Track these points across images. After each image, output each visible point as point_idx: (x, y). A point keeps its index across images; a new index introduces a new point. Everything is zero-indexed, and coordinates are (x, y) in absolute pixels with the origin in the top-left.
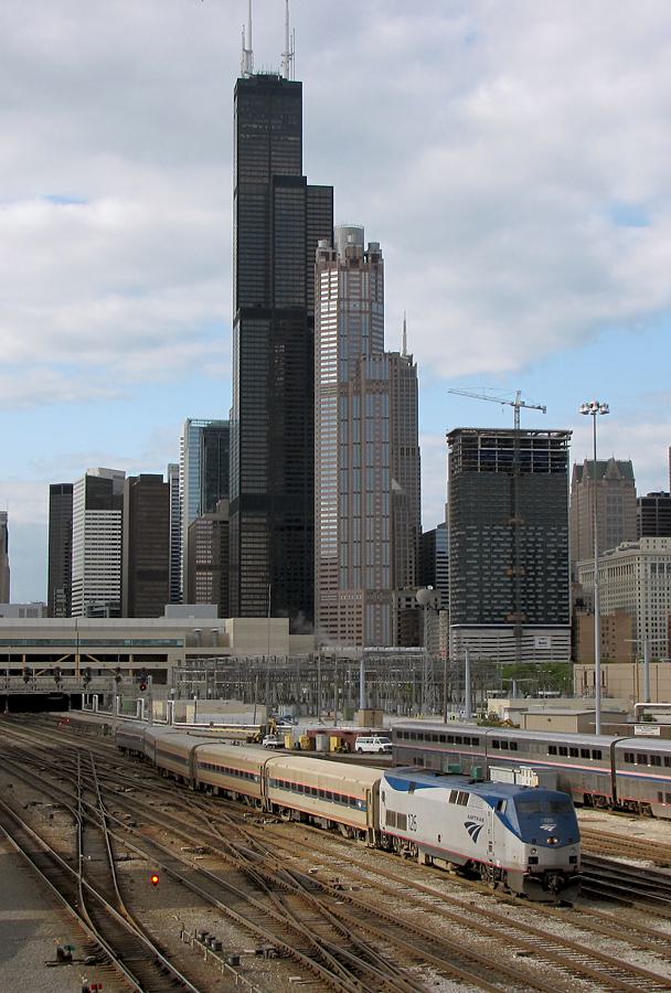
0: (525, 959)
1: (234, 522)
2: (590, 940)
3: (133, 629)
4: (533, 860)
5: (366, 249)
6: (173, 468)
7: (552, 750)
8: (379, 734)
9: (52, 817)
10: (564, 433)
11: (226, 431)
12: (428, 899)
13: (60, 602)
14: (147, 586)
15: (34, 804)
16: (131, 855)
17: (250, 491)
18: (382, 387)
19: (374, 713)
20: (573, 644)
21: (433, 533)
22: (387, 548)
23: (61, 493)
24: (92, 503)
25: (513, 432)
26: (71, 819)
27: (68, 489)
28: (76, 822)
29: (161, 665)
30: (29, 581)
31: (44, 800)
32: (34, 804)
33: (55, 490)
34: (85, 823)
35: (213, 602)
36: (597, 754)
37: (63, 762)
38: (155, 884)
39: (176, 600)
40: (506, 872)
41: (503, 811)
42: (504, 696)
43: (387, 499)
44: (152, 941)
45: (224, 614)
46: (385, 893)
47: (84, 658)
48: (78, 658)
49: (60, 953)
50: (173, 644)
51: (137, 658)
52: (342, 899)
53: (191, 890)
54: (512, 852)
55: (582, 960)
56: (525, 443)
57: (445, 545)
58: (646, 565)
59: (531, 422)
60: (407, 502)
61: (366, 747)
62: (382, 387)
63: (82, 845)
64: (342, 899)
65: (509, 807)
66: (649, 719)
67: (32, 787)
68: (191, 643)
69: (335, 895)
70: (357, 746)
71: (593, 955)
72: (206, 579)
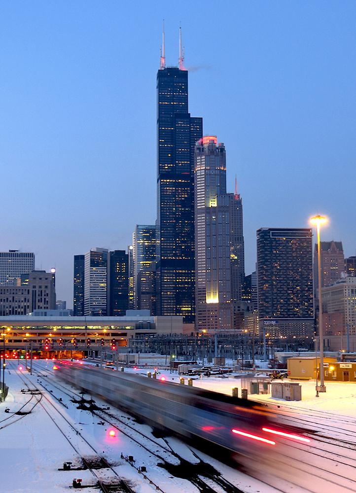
14: (117, 302)
21: (250, 276)
23: (79, 259)
24: (93, 263)
27: (82, 257)
33: (76, 258)
57: (255, 282)
58: (349, 290)
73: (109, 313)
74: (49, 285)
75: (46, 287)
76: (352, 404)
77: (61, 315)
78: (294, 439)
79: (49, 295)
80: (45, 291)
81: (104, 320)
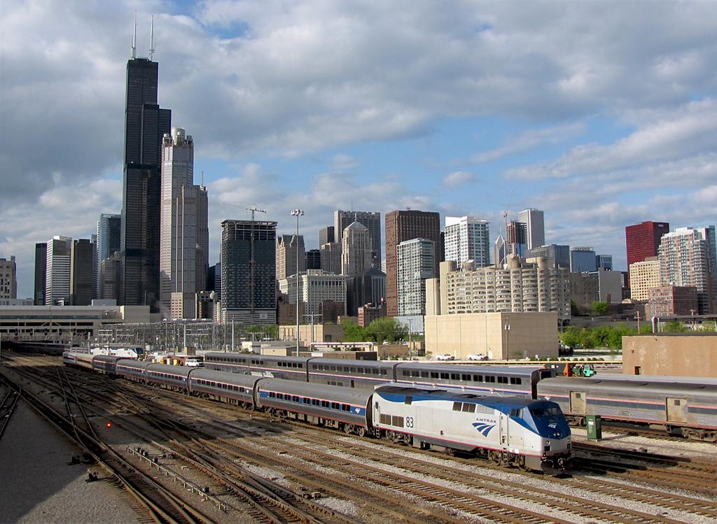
0: (284, 455)
1: (123, 260)
2: (310, 446)
3: (28, 311)
4: (547, 448)
5: (186, 138)
6: (94, 237)
7: (280, 364)
8: (196, 358)
9: (52, 397)
10: (274, 223)
11: (120, 219)
12: (234, 430)
13: (40, 298)
14: (84, 292)
15: (43, 392)
16: (94, 414)
17: (130, 247)
18: (192, 201)
19: (191, 350)
20: (277, 316)
21: (214, 267)
22: (193, 274)
23: (41, 248)
24: (56, 252)
25: (251, 222)
26: (61, 399)
27: (45, 245)
28: (63, 400)
29: (90, 327)
30: (26, 288)
31: (46, 390)
32: (43, 392)
33: (38, 246)
34: (69, 400)
35: (112, 298)
36: (300, 366)
37: (51, 373)
38: (109, 427)
39: (95, 298)
40: (524, 457)
41: (521, 416)
42: (248, 340)
43: (193, 252)
44: (115, 452)
45: (119, 304)
46: (379, 460)
47: (54, 324)
48: (51, 324)
49: (74, 458)
50: (96, 317)
51: (79, 324)
52: (195, 431)
53: (126, 430)
54: (530, 442)
55: (309, 455)
56: (256, 227)
57: (222, 274)
59: (260, 217)
60: (203, 254)
61: (190, 364)
62: (192, 201)
63: (69, 410)
64: (195, 431)
65: (526, 414)
66: (316, 349)
67: (38, 383)
68: (104, 317)
69: (192, 430)
70: (186, 363)
71: (313, 452)
72: (109, 289)
73: (71, 303)
74: (11, 274)
75: (7, 275)
76: (637, 370)
77: (24, 305)
78: (609, 385)
79: (10, 284)
80: (6, 280)
81: (88, 309)
